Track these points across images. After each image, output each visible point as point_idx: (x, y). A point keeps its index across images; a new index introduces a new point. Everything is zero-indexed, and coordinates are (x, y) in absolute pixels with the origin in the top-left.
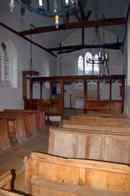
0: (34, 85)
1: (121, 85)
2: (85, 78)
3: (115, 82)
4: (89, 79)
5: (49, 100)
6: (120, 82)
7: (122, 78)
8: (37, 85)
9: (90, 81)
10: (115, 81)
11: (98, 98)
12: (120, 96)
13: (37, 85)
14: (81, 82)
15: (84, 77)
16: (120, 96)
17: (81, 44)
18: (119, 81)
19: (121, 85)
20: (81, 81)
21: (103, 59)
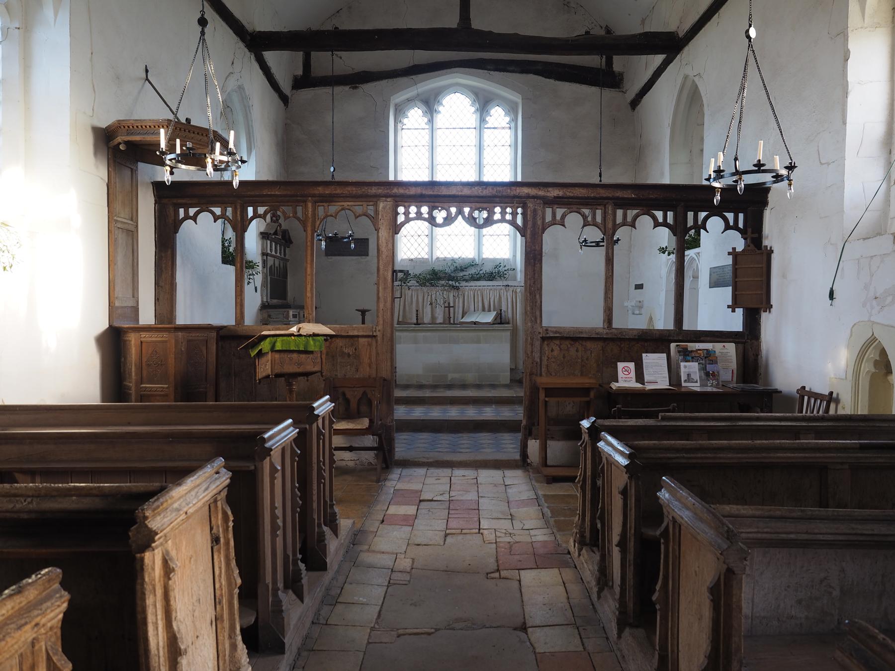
0: (551, 238)
1: (740, 244)
2: (534, 197)
3: (194, 218)
4: (625, 204)
5: (516, 381)
6: (735, 227)
7: (747, 204)
8: (203, 233)
9: (563, 217)
10: (706, 218)
11: (609, 319)
12: (733, 307)
13: (651, 237)
14: (503, 220)
15: (526, 190)
16: (733, 307)
17: (455, 26)
18: (585, 217)
19: (740, 244)
20: (508, 217)
21: (178, 141)
